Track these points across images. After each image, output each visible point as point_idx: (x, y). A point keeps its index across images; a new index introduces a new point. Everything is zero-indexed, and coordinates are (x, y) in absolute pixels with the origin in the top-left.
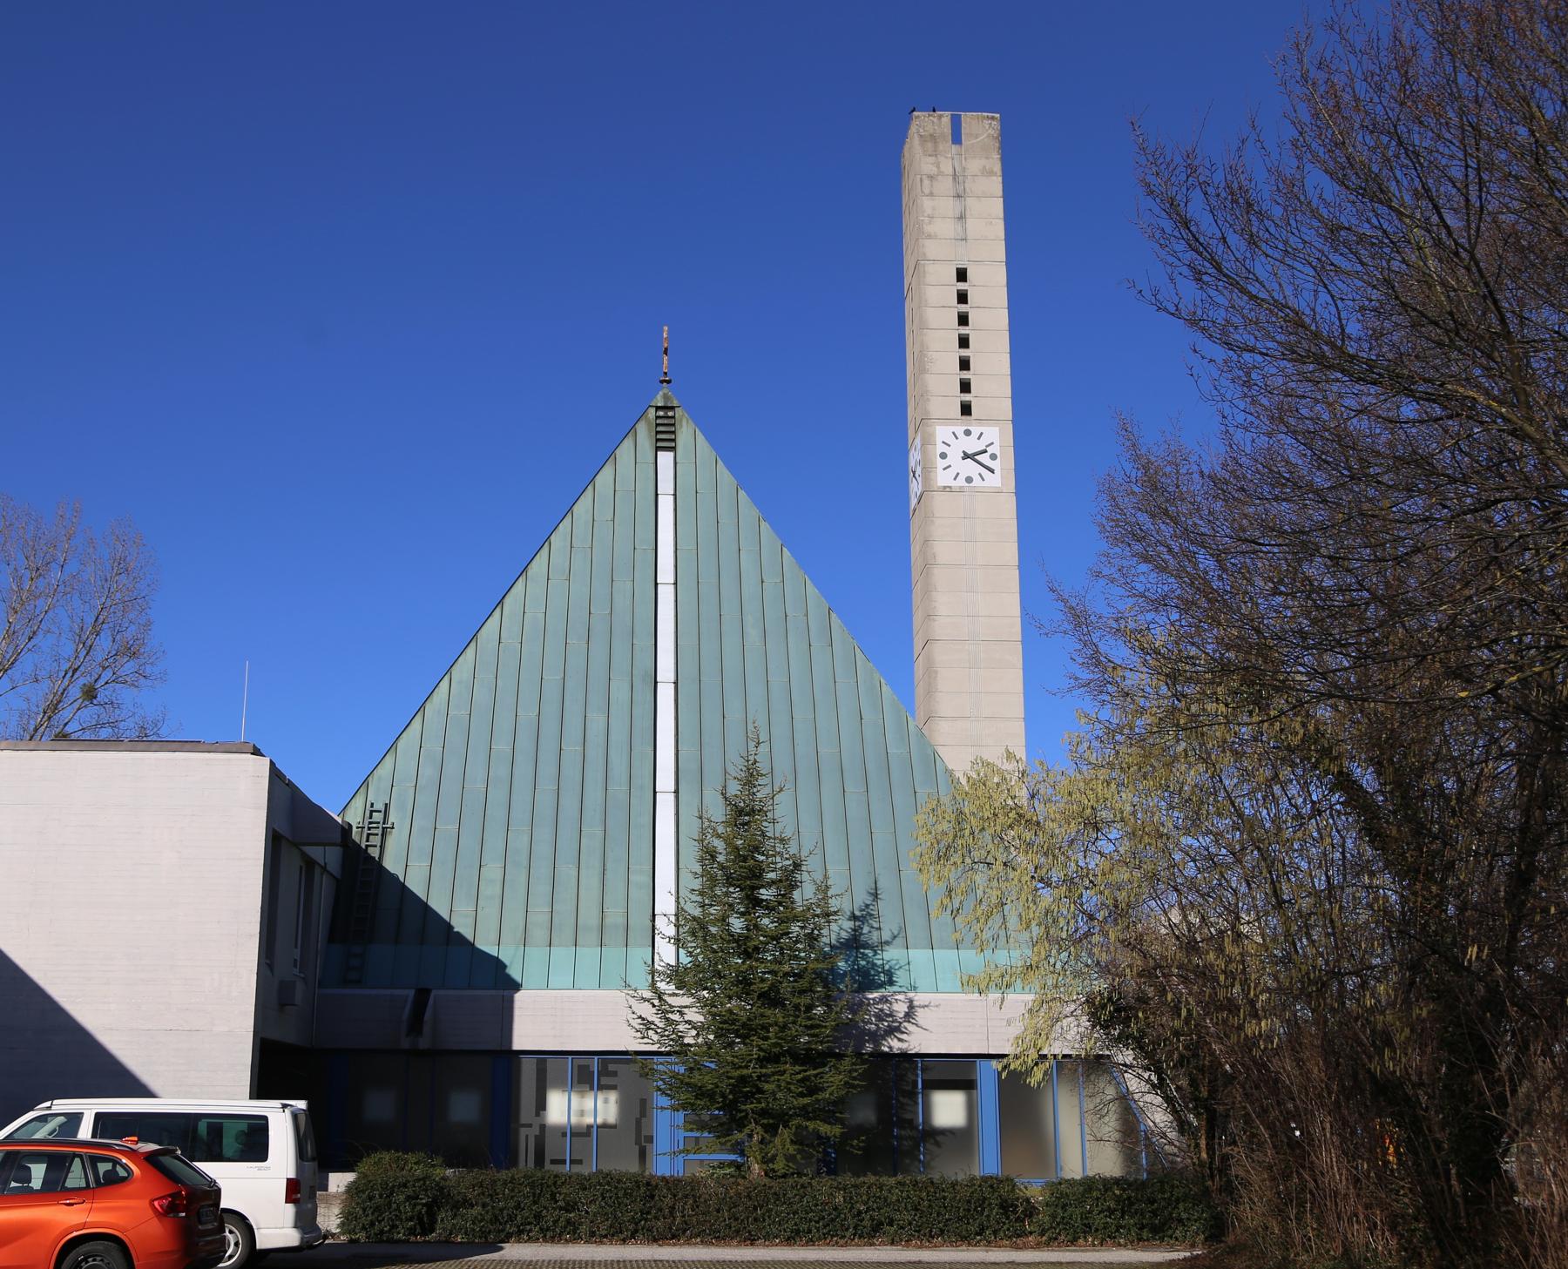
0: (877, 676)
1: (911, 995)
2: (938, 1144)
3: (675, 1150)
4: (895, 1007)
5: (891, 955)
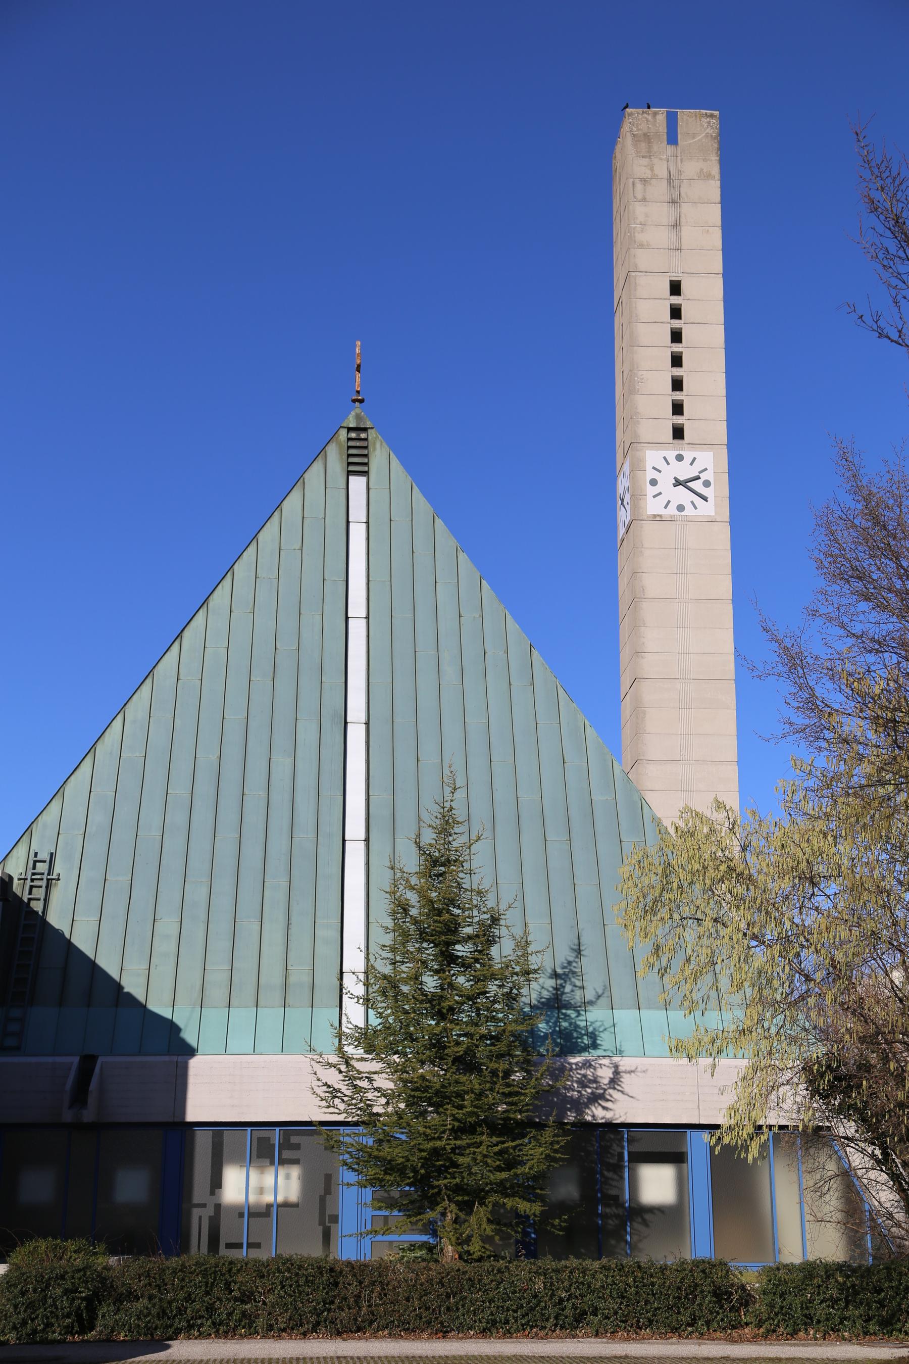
0: (580, 717)
1: (616, 1059)
2: (645, 1223)
3: (364, 1231)
4: (600, 1072)
5: (595, 1016)
